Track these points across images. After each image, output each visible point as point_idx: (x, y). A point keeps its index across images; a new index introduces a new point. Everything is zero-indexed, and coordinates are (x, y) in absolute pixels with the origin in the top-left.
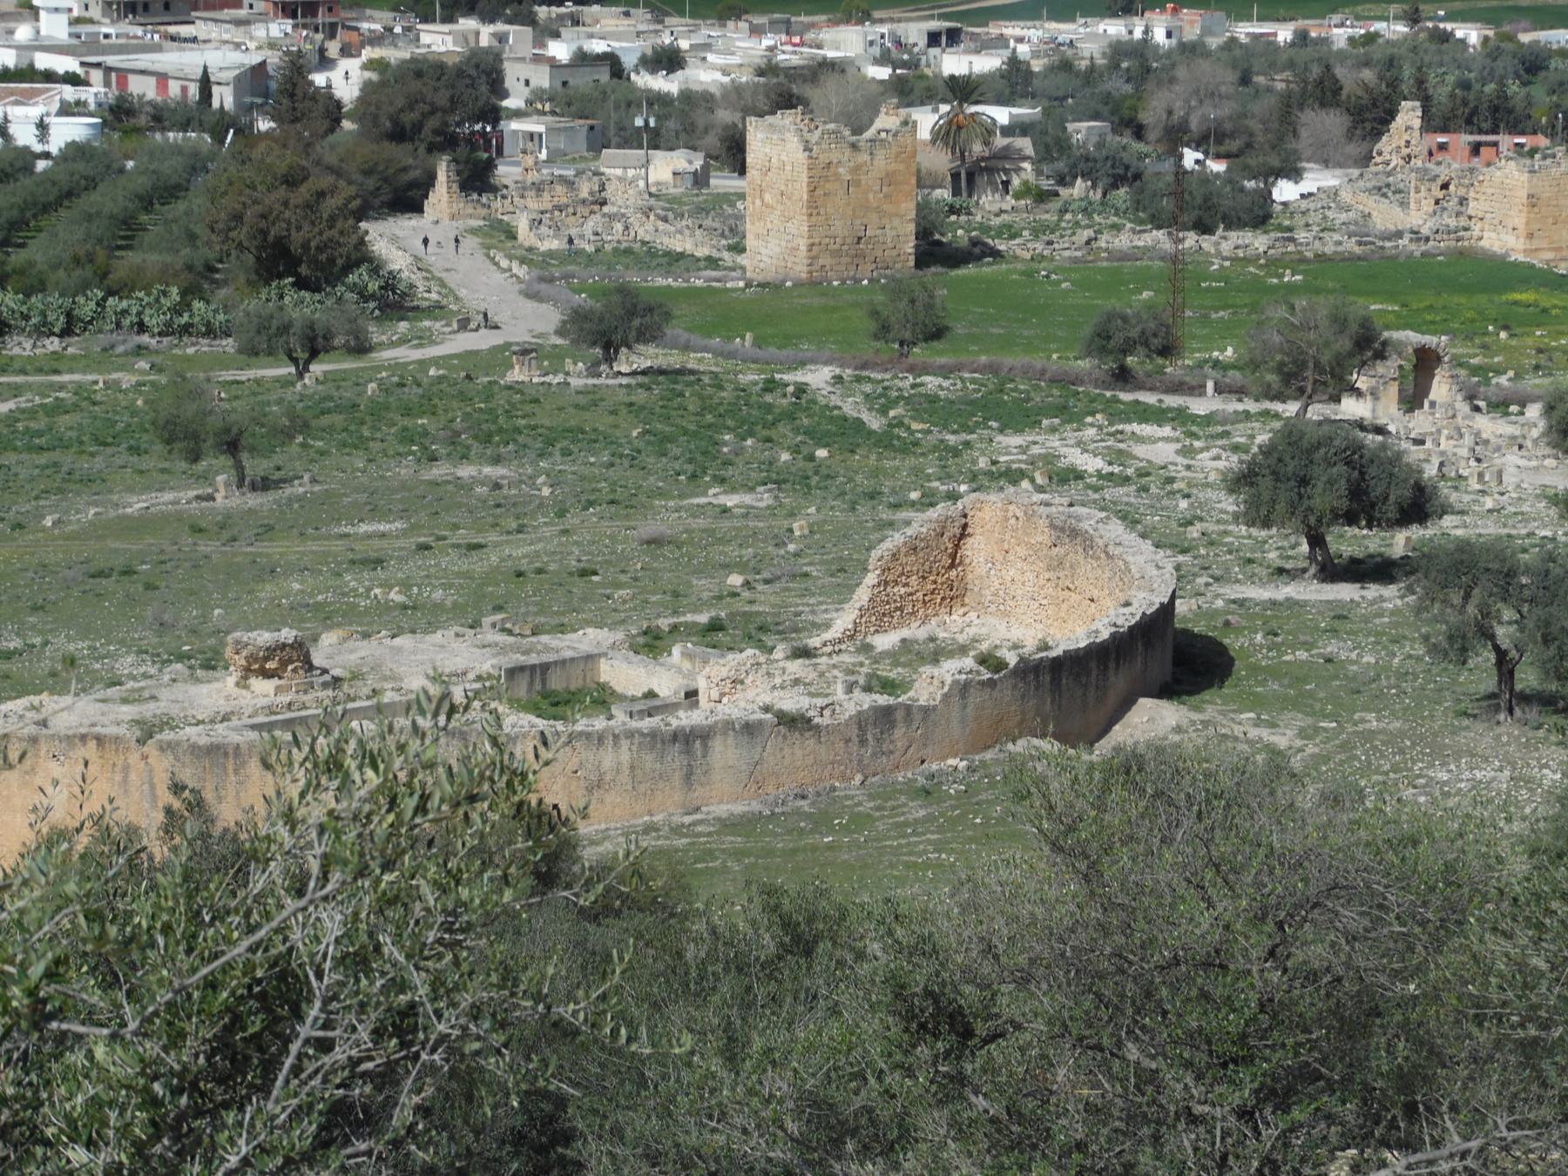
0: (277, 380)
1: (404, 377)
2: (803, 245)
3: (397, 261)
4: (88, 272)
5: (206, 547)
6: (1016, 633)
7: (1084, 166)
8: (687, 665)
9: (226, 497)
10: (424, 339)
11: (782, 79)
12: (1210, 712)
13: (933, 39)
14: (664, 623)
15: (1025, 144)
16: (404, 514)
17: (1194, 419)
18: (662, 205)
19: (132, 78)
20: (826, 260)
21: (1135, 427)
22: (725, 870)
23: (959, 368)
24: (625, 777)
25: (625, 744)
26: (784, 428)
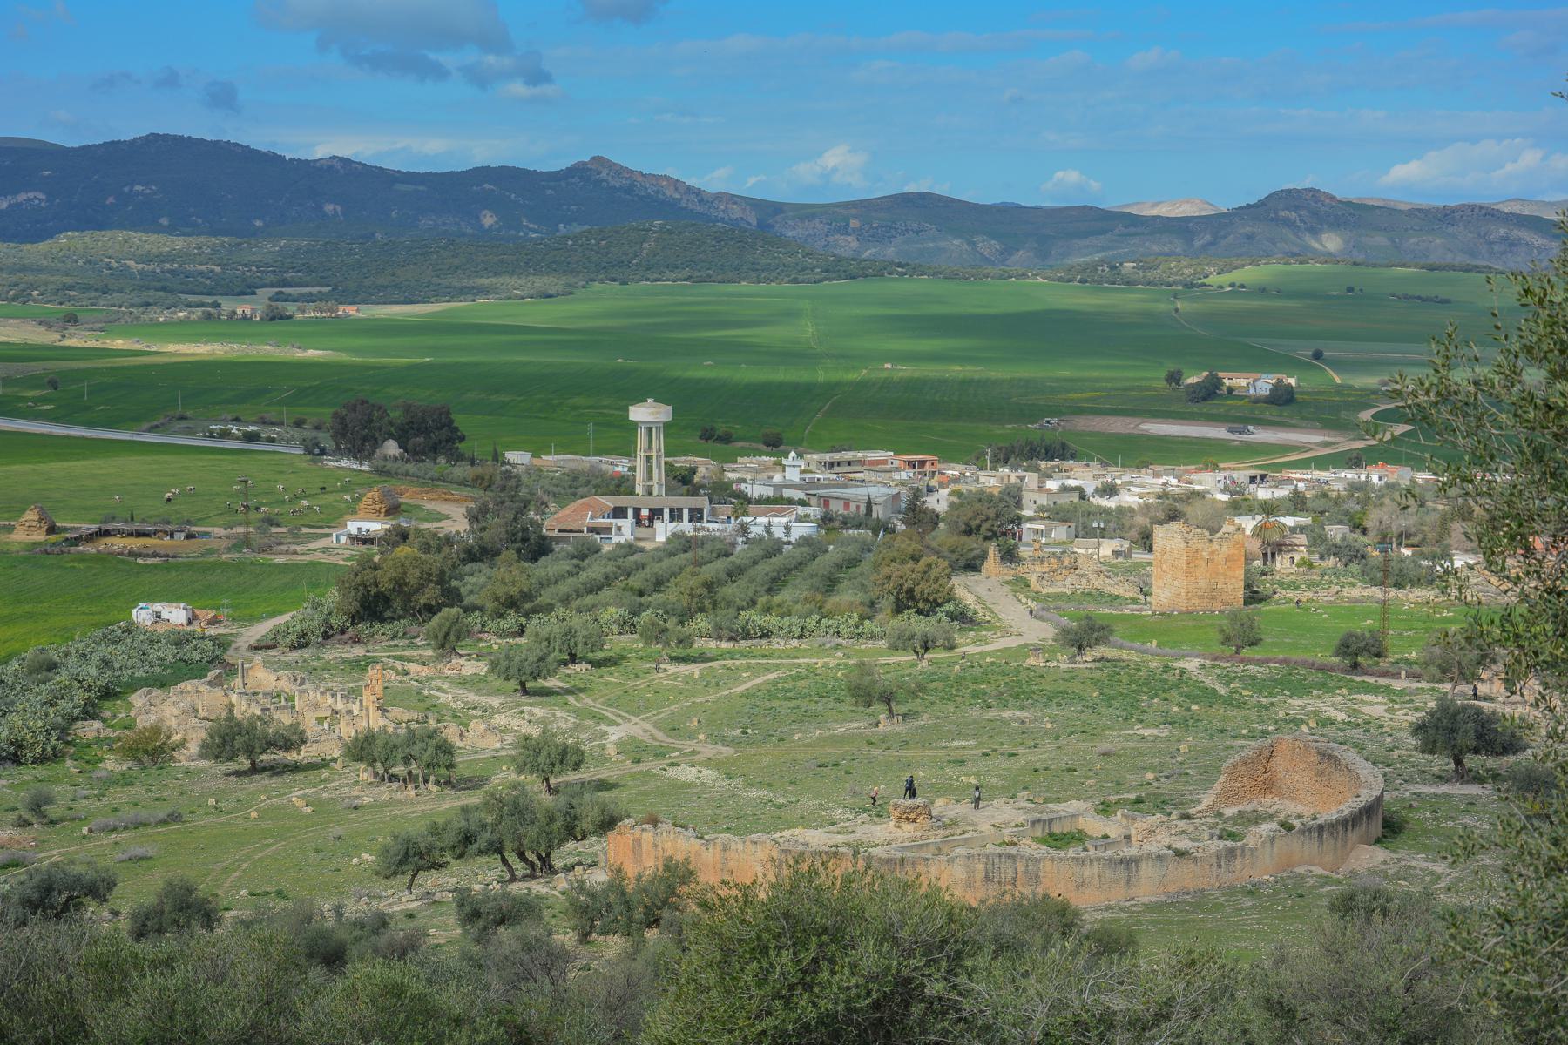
0: (907, 663)
1: (972, 662)
2: (1183, 592)
3: (969, 599)
4: (812, 605)
5: (875, 752)
6: (1300, 809)
7: (1335, 550)
8: (1124, 821)
9: (885, 726)
10: (982, 641)
11: (1170, 501)
12: (1402, 853)
13: (1253, 479)
14: (1113, 798)
15: (1302, 539)
16: (975, 736)
17: (1394, 692)
18: (1107, 570)
19: (832, 502)
20: (1196, 601)
21: (1363, 696)
22: (1148, 931)
23: (1268, 661)
24: (1095, 881)
25: (1096, 864)
26: (1174, 693)
